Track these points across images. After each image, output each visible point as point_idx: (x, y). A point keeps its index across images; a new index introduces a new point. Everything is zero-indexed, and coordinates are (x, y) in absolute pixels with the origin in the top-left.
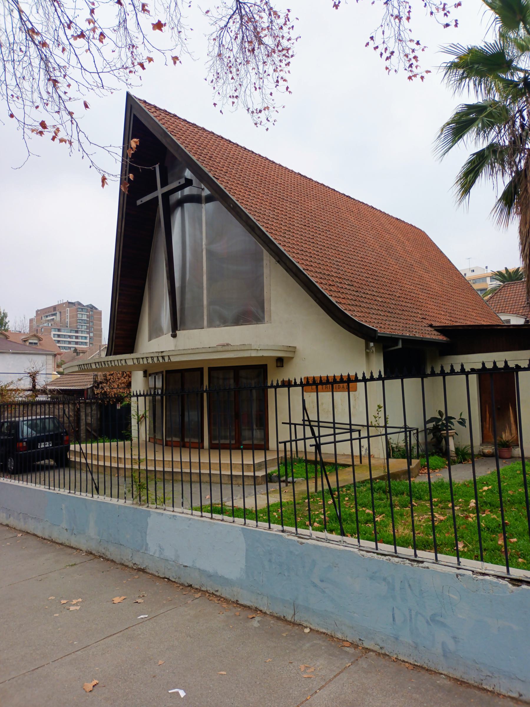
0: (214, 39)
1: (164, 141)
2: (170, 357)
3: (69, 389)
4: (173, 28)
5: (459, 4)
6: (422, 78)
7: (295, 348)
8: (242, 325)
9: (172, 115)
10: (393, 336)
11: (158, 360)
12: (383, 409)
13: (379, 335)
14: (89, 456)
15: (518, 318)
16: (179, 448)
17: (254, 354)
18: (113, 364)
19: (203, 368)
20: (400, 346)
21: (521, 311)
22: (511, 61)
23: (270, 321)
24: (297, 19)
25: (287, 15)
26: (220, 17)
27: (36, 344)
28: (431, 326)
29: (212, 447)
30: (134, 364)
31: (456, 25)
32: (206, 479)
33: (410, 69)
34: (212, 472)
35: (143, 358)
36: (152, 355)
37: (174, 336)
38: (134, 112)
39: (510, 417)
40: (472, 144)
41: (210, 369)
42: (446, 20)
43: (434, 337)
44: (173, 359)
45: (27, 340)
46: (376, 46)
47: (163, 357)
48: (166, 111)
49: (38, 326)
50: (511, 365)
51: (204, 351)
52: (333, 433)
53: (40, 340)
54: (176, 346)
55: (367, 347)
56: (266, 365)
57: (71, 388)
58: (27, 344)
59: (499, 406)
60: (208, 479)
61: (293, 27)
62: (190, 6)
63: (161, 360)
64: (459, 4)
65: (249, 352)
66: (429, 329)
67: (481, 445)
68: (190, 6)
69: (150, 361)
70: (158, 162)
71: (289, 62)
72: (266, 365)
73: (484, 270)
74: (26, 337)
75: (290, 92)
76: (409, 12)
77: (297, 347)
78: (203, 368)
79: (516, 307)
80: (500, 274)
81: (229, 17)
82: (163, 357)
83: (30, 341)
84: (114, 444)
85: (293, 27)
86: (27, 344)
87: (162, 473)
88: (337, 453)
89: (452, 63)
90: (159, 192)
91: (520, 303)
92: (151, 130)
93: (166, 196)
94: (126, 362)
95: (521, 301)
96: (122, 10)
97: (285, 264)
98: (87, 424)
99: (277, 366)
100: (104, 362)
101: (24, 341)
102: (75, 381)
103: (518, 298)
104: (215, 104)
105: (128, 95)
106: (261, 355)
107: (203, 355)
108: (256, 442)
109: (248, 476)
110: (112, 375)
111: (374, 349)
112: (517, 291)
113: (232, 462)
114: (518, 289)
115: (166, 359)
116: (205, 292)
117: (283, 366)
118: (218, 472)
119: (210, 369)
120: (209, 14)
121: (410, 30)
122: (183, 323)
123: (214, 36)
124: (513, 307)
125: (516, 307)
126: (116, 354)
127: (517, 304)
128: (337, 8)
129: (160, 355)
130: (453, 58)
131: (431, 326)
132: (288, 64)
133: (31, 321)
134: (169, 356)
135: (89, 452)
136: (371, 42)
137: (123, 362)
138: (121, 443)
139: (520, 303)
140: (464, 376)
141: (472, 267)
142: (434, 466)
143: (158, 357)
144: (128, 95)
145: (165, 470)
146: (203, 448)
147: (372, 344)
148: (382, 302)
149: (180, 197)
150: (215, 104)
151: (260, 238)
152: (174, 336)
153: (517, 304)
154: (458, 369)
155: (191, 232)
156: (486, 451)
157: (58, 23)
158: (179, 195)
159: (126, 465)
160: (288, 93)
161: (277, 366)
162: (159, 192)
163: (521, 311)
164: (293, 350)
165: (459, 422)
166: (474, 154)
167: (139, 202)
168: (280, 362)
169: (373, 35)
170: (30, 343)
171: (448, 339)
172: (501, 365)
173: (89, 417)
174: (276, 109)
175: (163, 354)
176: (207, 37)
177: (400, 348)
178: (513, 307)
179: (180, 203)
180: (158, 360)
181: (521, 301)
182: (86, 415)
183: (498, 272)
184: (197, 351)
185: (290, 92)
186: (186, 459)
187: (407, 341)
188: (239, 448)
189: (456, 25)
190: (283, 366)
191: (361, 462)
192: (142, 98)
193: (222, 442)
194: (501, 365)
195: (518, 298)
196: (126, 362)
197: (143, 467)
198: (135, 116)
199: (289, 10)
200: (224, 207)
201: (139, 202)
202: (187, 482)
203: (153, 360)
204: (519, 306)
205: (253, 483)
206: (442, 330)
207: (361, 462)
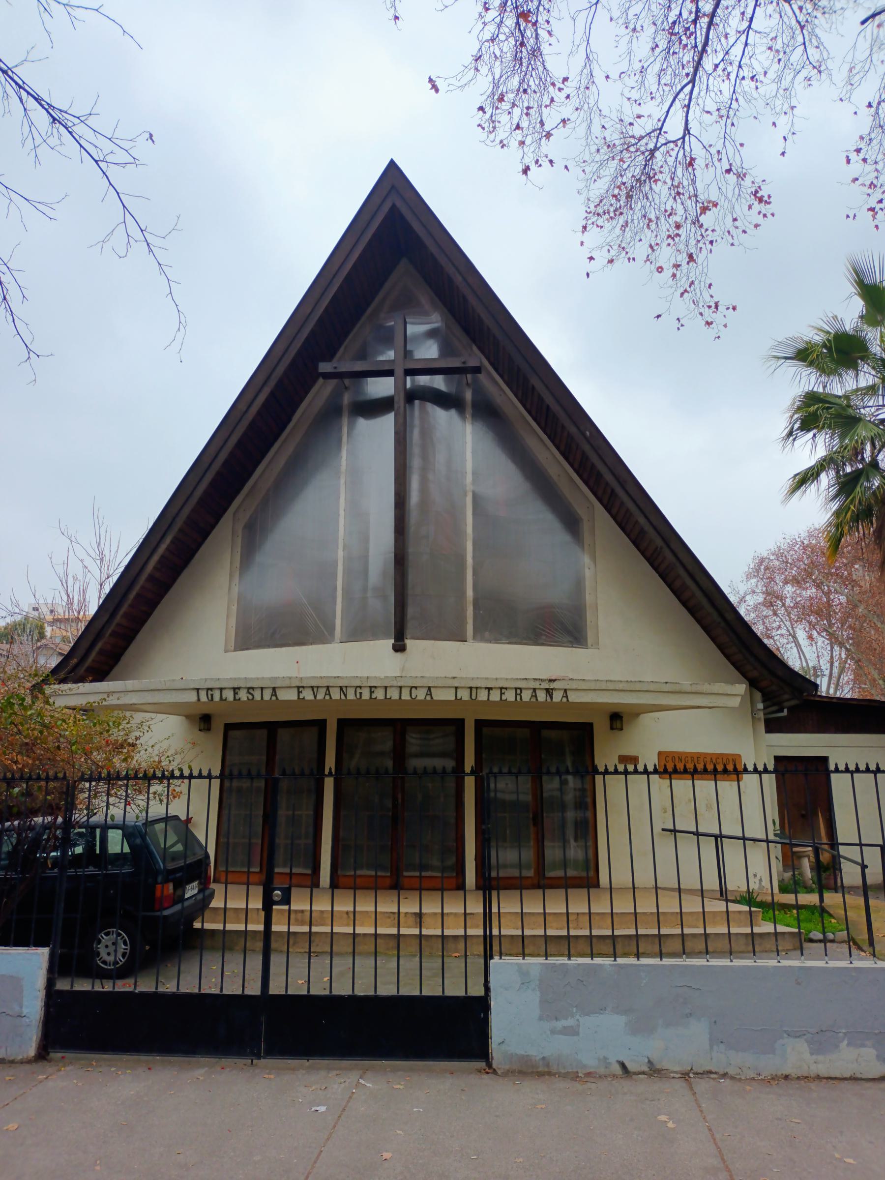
6: (682, 325)
19: (325, 721)
23: (596, 645)
36: (536, 685)
37: (399, 648)
39: (819, 828)
41: (343, 724)
44: (573, 697)
47: (549, 692)
51: (652, 687)
54: (403, 669)
59: (804, 812)
63: (542, 696)
78: (325, 721)
82: (549, 692)
87: (703, 938)
99: (612, 728)
107: (647, 695)
108: (571, 873)
109: (694, 936)
115: (557, 697)
117: (200, 730)
129: (546, 685)
134: (341, 688)
145: (615, 933)
146: (597, 885)
152: (399, 648)
157: (794, 22)
159: (468, 930)
161: (612, 728)
168: (617, 719)
175: (552, 686)
184: (638, 687)
188: (538, 886)
190: (622, 729)
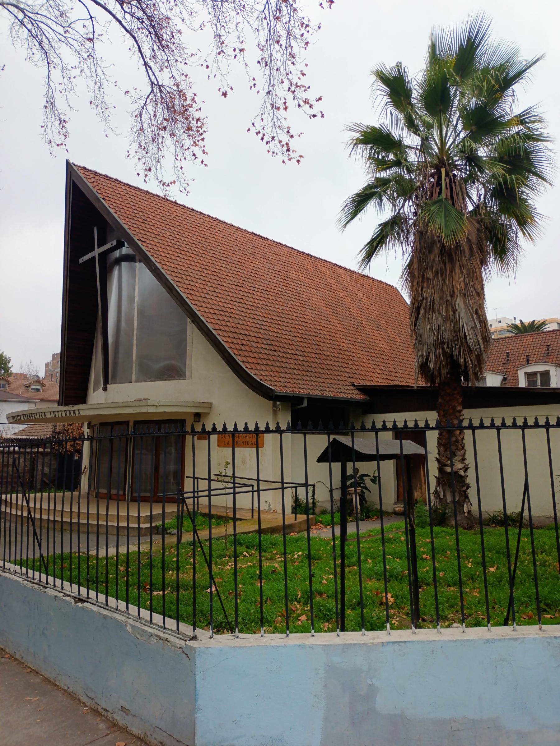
0: (136, 116)
1: (97, 206)
2: (80, 411)
3: (26, 439)
4: (98, 106)
5: (320, 99)
7: (211, 404)
8: (166, 380)
9: (113, 180)
10: (295, 395)
11: (70, 414)
12: (231, 466)
13: (276, 394)
14: (14, 506)
15: (494, 375)
16: (106, 501)
17: (151, 410)
18: (36, 417)
20: (305, 405)
21: (500, 368)
22: (400, 141)
24: (203, 102)
25: (194, 98)
26: (139, 97)
27: (38, 389)
28: (353, 385)
29: (134, 499)
30: (52, 417)
31: (323, 116)
32: (102, 530)
33: (288, 153)
34: (90, 522)
35: (58, 412)
37: (105, 389)
38: (73, 178)
40: (376, 215)
42: (312, 112)
43: (349, 396)
45: (29, 386)
46: (257, 131)
48: (107, 176)
49: (54, 371)
50: (422, 424)
52: (281, 487)
53: (43, 386)
54: (106, 399)
55: (275, 406)
56: (185, 420)
57: (28, 437)
58: (30, 389)
60: (95, 529)
61: (200, 109)
62: (116, 86)
64: (320, 99)
65: (146, 407)
66: (352, 387)
67: (395, 503)
68: (116, 86)
69: (64, 414)
70: (94, 224)
71: (204, 138)
72: (185, 420)
73: (512, 320)
74: (29, 382)
75: (206, 165)
76: (285, 103)
77: (214, 403)
79: (496, 363)
80: (515, 326)
81: (146, 97)
83: (33, 387)
84: (59, 494)
85: (200, 109)
86: (30, 389)
88: (237, 507)
89: (357, 139)
90: (97, 252)
91: (500, 360)
92: (87, 195)
93: (103, 256)
94: (45, 415)
95: (501, 357)
96: (50, 91)
97: (198, 323)
98: (43, 474)
100: (29, 414)
101: (27, 387)
102: (33, 431)
103: (499, 355)
104: (138, 174)
105: (68, 163)
106: (163, 411)
110: (71, 425)
111: (280, 407)
112: (499, 347)
113: (90, 512)
114: (500, 345)
115: (77, 412)
116: (135, 347)
118: (115, 524)
119: (136, 422)
120: (129, 94)
121: (285, 119)
122: (114, 376)
123: (136, 113)
124: (493, 364)
125: (496, 363)
126: (66, 404)
127: (497, 361)
128: (225, 97)
130: (357, 135)
131: (353, 385)
132: (203, 139)
133: (47, 365)
135: (14, 501)
136: (252, 128)
137: (43, 415)
138: (67, 494)
139: (500, 360)
140: (495, 431)
141: (499, 317)
142: (327, 522)
143: (70, 411)
144: (68, 163)
147: (278, 403)
148: (304, 361)
149: (118, 256)
150: (138, 174)
151: (177, 299)
152: (105, 389)
153: (497, 361)
154: (487, 423)
155: (129, 290)
156: (397, 509)
158: (117, 254)
160: (203, 165)
162: (97, 252)
163: (500, 368)
164: (210, 406)
165: (372, 480)
166: (380, 225)
167: (81, 261)
168: (198, 416)
169: (253, 122)
170: (33, 389)
171: (368, 398)
172: (411, 425)
173: (45, 468)
174: (186, 182)
176: (130, 114)
177: (305, 407)
178: (493, 364)
179: (118, 261)
180: (70, 414)
181: (501, 357)
182: (43, 465)
183: (512, 324)
184: (101, 406)
185: (206, 165)
186: (113, 512)
187: (311, 400)
189: (323, 116)
191: (252, 517)
192: (82, 165)
193: (143, 494)
194: (411, 425)
195: (499, 355)
196: (45, 415)
197: (51, 518)
198: (73, 181)
199: (195, 95)
200: (147, 269)
201: (81, 261)
202: (84, 533)
203: (66, 413)
204: (499, 363)
205: (116, 533)
206: (363, 389)
207: (252, 517)
